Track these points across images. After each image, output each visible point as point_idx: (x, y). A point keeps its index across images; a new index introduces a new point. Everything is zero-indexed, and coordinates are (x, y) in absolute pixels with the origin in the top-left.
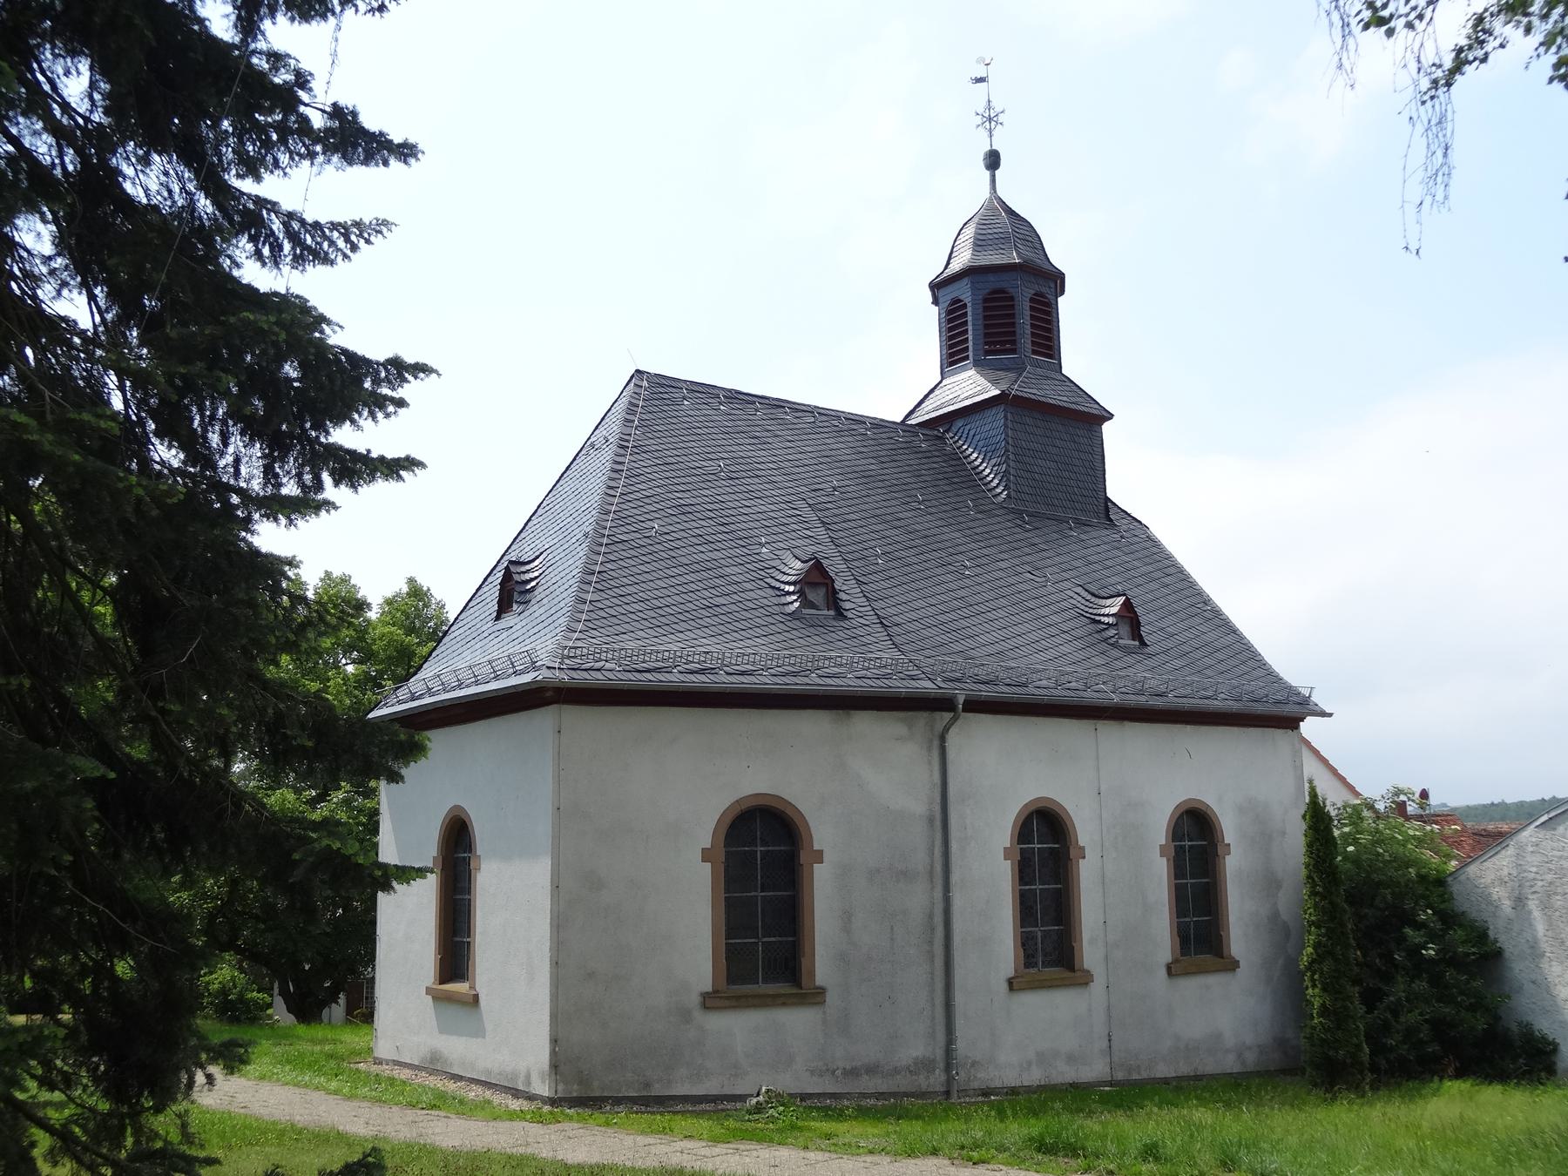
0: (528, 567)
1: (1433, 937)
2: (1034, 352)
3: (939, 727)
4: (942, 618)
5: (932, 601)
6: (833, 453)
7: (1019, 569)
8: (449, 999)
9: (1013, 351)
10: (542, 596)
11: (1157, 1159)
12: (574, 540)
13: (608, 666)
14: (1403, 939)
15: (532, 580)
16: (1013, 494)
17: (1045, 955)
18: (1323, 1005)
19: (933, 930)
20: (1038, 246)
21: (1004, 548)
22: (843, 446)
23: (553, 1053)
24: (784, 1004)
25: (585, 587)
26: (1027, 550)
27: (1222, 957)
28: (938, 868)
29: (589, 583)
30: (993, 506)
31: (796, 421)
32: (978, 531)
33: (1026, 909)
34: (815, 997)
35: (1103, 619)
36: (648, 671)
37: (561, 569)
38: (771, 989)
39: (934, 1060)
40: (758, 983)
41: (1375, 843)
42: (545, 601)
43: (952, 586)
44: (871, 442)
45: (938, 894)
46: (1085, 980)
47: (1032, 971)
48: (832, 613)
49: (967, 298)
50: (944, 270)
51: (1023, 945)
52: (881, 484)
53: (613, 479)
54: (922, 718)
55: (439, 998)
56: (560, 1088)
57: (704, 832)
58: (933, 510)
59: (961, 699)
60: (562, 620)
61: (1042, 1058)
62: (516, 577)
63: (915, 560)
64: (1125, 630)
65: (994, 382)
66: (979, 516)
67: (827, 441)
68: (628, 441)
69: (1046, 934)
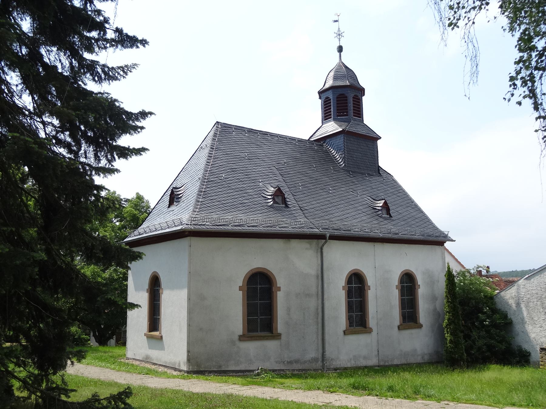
0: (179, 190)
1: (488, 317)
2: (354, 116)
3: (320, 245)
4: (322, 207)
10: (184, 199)
11: (393, 391)
12: (195, 180)
13: (207, 224)
14: (478, 318)
15: (181, 194)
16: (346, 164)
17: (356, 323)
18: (451, 340)
19: (318, 314)
20: (356, 79)
21: (343, 183)
22: (288, 148)
23: (188, 356)
26: (351, 184)
28: (320, 293)
29: (201, 195)
30: (340, 169)
31: (272, 139)
33: (350, 307)
34: (278, 336)
35: (377, 208)
36: (221, 225)
37: (191, 190)
38: (263, 334)
39: (318, 358)
42: (185, 201)
46: (370, 331)
48: (284, 206)
49: (331, 97)
56: (190, 367)
57: (240, 280)
59: (328, 235)
62: (175, 193)
63: (313, 187)
64: (384, 211)
65: (340, 126)
66: (335, 172)
68: (214, 146)
69: (357, 316)
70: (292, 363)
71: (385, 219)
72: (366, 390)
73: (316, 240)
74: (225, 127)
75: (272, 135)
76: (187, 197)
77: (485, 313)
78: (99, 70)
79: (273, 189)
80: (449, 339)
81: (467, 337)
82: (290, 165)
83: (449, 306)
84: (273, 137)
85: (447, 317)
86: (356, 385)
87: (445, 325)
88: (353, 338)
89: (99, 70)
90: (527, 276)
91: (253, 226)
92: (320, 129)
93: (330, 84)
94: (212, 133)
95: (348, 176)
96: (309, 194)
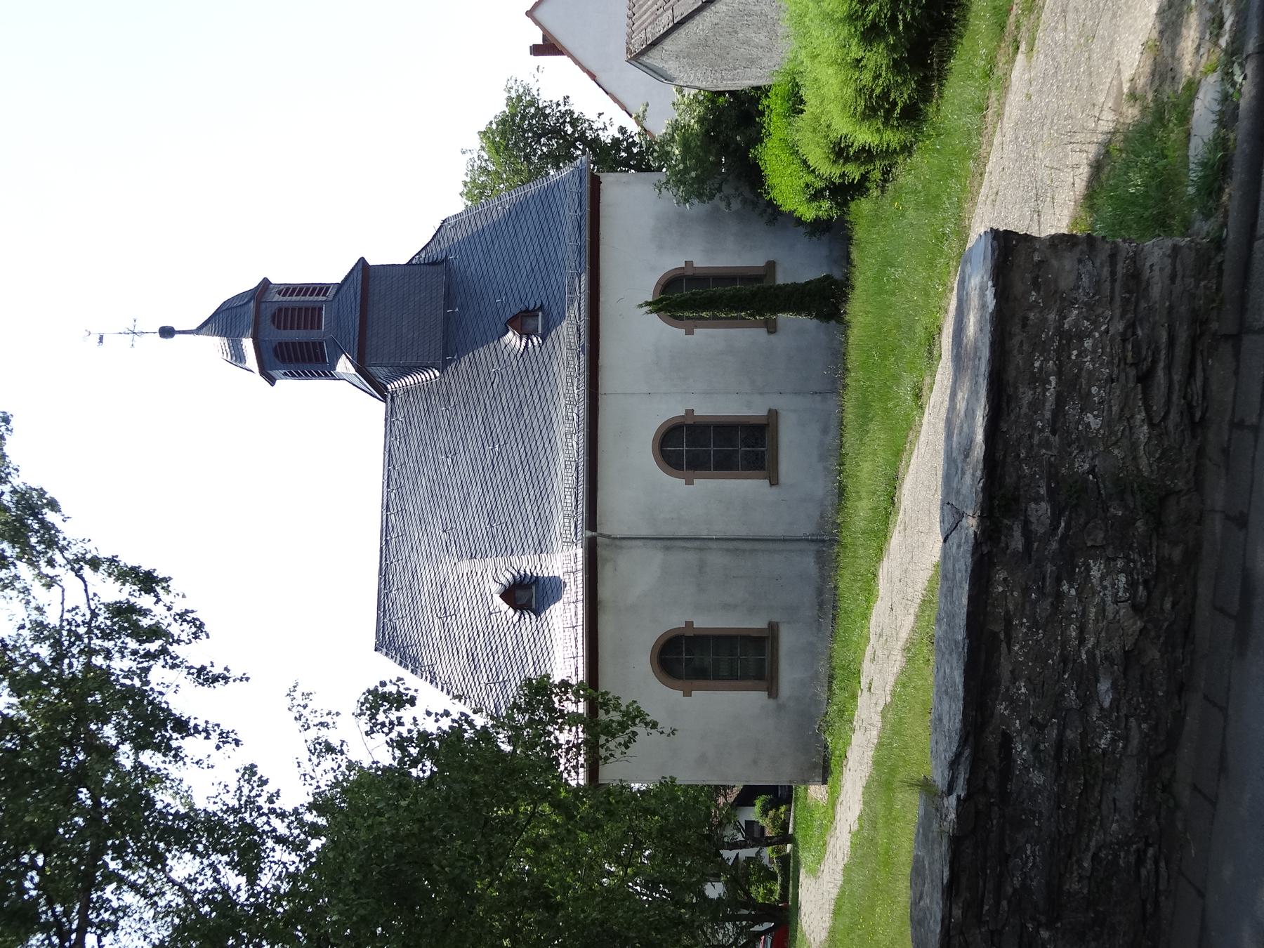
2: (319, 327)
19: (737, 550)
27: (765, 275)
28: (697, 544)
34: (773, 628)
39: (818, 551)
40: (763, 452)
45: (714, 545)
46: (773, 415)
48: (534, 587)
54: (601, 552)
56: (817, 779)
57: (674, 484)
59: (589, 534)
70: (822, 601)
73: (599, 550)
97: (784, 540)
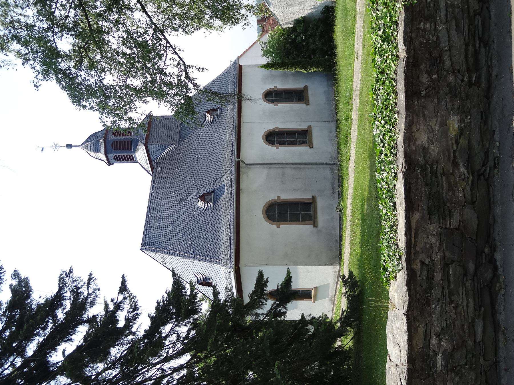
0: (199, 278)
1: (299, 35)
2: (131, 135)
3: (244, 165)
4: (213, 164)
5: (208, 167)
6: (164, 194)
7: (197, 142)
8: (315, 295)
9: (131, 142)
10: (208, 273)
11: (348, 119)
12: (192, 265)
13: (229, 252)
14: (299, 43)
15: (203, 277)
16: (174, 143)
17: (304, 138)
18: (316, 68)
19: (297, 168)
20: (97, 133)
21: (191, 146)
22: (161, 191)
23: (328, 265)
24: (316, 206)
25: (207, 260)
26: (191, 139)
28: (281, 166)
29: (206, 259)
30: (178, 149)
31: (154, 205)
32: (186, 154)
33: (292, 143)
34: (314, 198)
35: (212, 119)
36: (230, 242)
37: (200, 268)
38: (312, 210)
40: (306, 141)
41: (273, 48)
42: (209, 272)
43: (204, 161)
44: (159, 183)
46: (310, 127)
47: (308, 142)
48: (213, 194)
49: (114, 155)
50: (104, 161)
51: (301, 144)
52: (173, 181)
53: (175, 255)
55: (315, 300)
56: (337, 263)
57: (273, 227)
58: (180, 166)
59: (237, 159)
60: (216, 266)
61: (331, 140)
62: (202, 281)
63: (196, 171)
64: (215, 113)
65: (141, 147)
66: (181, 153)
67: (160, 196)
68: (163, 251)
69: (298, 138)
70: (334, 187)
71: (221, 112)
72: (348, 136)
73: (241, 169)
74: (145, 243)
75: (150, 205)
76: (206, 270)
77: (296, 37)
78: (132, 314)
79: (199, 203)
80: (315, 69)
81: (314, 52)
82: (177, 190)
83: (291, 68)
84: (152, 204)
85: (299, 70)
86: (345, 142)
87: (305, 72)
88: (315, 141)
89: (132, 314)
90: (267, 5)
91: (231, 217)
92: (142, 164)
93: (102, 156)
94: (151, 253)
95: (184, 142)
96: (202, 174)
97: (316, 164)
